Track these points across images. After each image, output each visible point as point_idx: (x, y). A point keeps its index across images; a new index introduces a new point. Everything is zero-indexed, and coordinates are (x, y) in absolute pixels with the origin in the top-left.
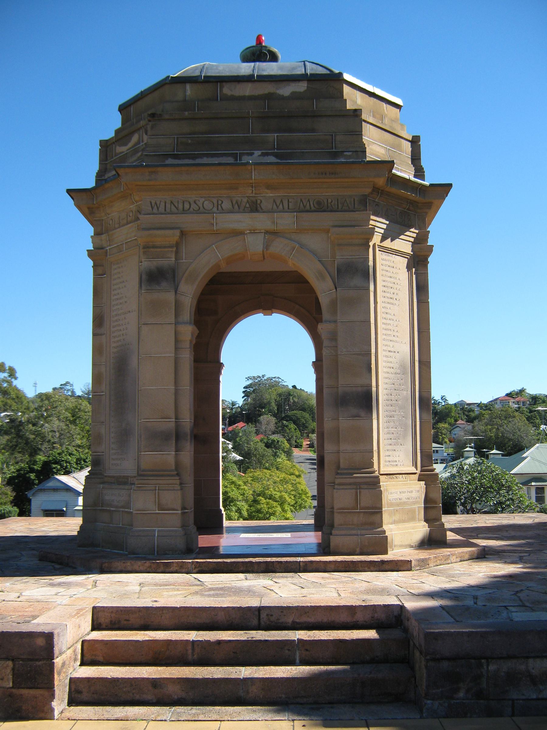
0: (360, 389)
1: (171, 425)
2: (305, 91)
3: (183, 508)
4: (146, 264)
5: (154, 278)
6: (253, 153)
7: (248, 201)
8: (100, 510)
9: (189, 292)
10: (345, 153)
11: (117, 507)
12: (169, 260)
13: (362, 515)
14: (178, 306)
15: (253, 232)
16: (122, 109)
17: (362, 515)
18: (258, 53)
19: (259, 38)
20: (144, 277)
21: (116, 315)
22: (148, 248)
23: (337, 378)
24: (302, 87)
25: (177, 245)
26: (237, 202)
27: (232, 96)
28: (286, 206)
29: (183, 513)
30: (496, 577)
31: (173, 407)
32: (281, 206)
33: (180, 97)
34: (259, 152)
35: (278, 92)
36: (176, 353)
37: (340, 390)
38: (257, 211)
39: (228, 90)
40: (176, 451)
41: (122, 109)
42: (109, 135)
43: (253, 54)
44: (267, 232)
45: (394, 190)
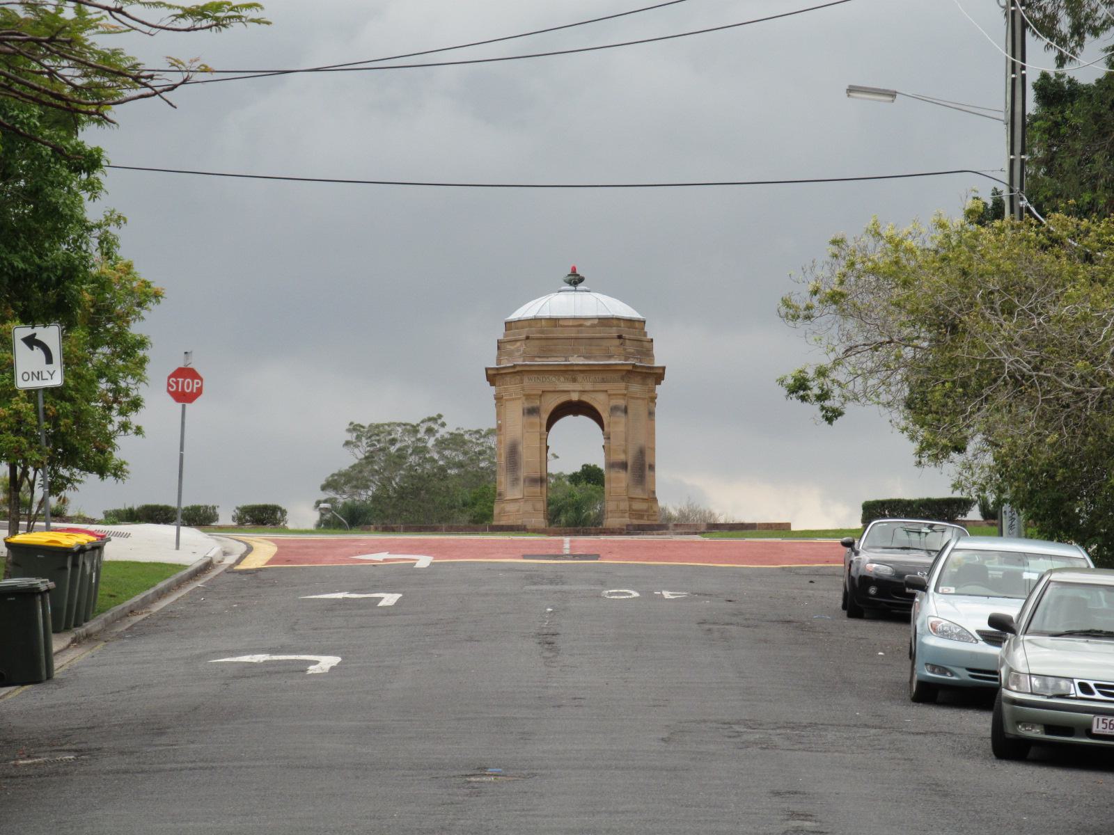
4: (527, 405)
12: (536, 403)
15: (574, 391)
19: (574, 269)
22: (528, 397)
24: (596, 322)
25: (541, 396)
39: (561, 323)
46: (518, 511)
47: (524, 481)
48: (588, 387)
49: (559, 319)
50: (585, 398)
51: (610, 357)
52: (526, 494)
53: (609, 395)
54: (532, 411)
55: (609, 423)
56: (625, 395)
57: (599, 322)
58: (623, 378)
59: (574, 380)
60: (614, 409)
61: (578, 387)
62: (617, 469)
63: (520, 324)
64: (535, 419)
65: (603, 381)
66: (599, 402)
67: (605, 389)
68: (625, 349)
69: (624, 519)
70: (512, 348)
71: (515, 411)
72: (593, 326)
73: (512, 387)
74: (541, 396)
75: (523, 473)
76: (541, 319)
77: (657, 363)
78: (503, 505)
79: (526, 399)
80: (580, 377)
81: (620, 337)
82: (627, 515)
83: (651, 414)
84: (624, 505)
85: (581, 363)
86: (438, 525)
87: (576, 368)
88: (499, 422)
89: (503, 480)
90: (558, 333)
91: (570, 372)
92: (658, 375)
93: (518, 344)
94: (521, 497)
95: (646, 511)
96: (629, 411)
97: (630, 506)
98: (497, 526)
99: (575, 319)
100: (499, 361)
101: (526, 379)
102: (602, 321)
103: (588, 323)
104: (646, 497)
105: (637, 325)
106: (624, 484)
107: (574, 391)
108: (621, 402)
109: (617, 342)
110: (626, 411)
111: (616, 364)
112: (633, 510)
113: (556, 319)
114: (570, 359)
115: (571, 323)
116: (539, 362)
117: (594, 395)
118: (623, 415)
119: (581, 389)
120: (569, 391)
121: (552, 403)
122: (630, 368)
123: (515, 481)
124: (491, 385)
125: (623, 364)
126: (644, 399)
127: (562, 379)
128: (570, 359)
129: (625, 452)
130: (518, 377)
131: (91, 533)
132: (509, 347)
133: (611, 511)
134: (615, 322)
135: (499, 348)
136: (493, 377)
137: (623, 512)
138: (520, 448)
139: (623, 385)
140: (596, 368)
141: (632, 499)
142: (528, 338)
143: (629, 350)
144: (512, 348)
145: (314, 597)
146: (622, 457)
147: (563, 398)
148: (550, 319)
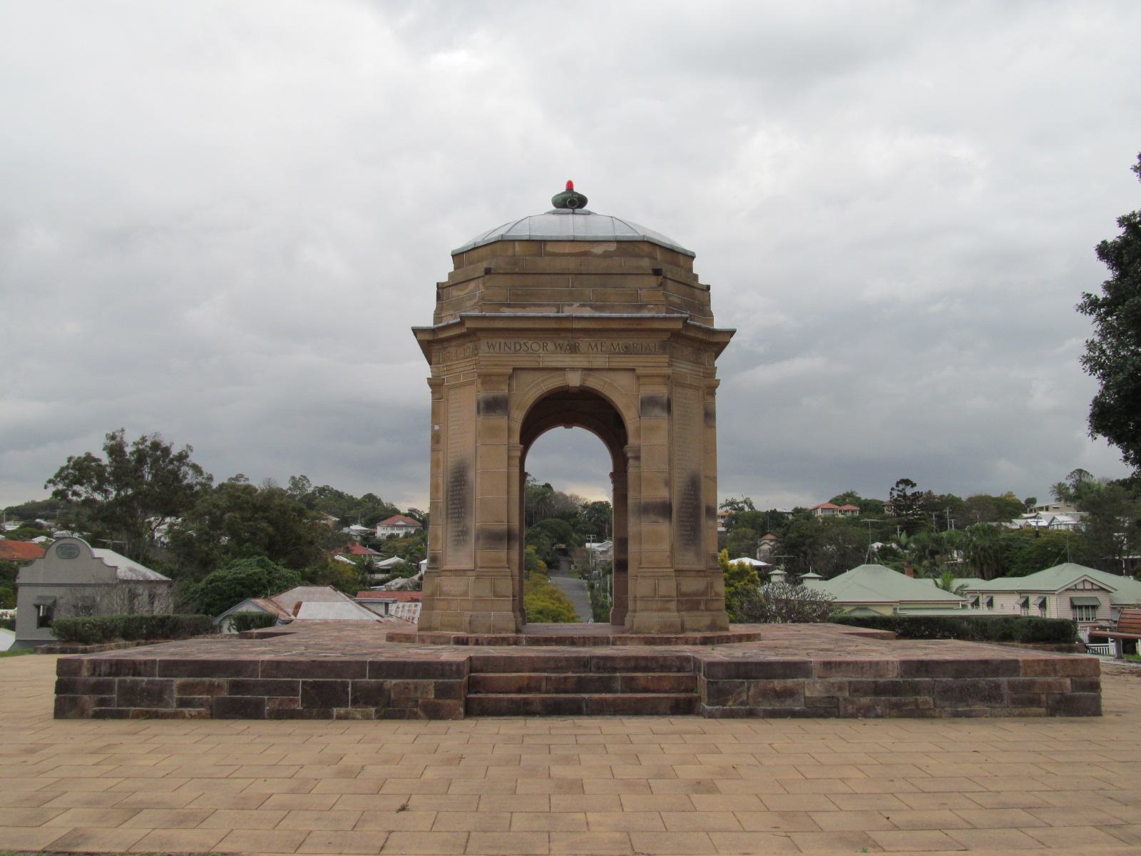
0: (658, 500)
1: (505, 527)
2: (615, 251)
3: (514, 596)
4: (484, 394)
5: (492, 406)
6: (572, 305)
7: (568, 345)
8: (438, 599)
9: (518, 416)
10: (649, 306)
11: (454, 596)
12: (502, 391)
13: (659, 602)
14: (509, 429)
15: (573, 369)
16: (457, 256)
17: (659, 602)
18: (571, 201)
19: (570, 185)
20: (482, 405)
21: (453, 434)
22: (486, 378)
23: (640, 492)
24: (613, 247)
25: (511, 377)
26: (559, 344)
27: (554, 253)
28: (599, 350)
29: (513, 600)
30: (558, 195)
31: (505, 511)
32: (595, 349)
33: (510, 253)
34: (578, 304)
35: (592, 250)
36: (508, 469)
37: (642, 502)
38: (576, 352)
39: (550, 248)
40: (508, 549)
41: (457, 256)
42: (444, 279)
43: (565, 200)
44: (585, 369)
45: (691, 334)
46: (465, 594)
47: (477, 538)
48: (600, 362)
49: (545, 241)
50: (594, 383)
51: (640, 307)
52: (479, 565)
53: (638, 377)
54: (492, 406)
55: (638, 430)
56: (668, 377)
57: (618, 248)
58: (664, 347)
59: (574, 349)
60: (648, 404)
61: (580, 361)
62: (654, 518)
63: (474, 254)
64: (500, 421)
65: (628, 351)
66: (622, 392)
67: (631, 365)
68: (666, 297)
69: (667, 614)
70: (461, 294)
71: (466, 401)
72: (607, 255)
73: (462, 364)
74: (511, 377)
75: (475, 523)
76: (514, 241)
77: (718, 324)
78: (438, 580)
79: (483, 383)
80: (584, 343)
81: (657, 272)
82: (673, 605)
83: (709, 416)
84: (667, 587)
85: (587, 315)
86: (936, 692)
87: (576, 325)
88: (437, 427)
89: (440, 533)
90: (544, 263)
91: (563, 333)
92: (716, 342)
93: (472, 285)
94: (471, 566)
95: (704, 593)
96: (674, 407)
97: (678, 585)
98: (520, 529)
99: (574, 241)
100: (438, 316)
101: (483, 346)
102: (624, 246)
103: (598, 250)
104: (702, 567)
105: (682, 260)
106: (666, 547)
107: (573, 369)
108: (661, 391)
109: (653, 281)
110: (668, 407)
111: (652, 319)
112: (684, 595)
113: (540, 241)
114: (566, 309)
115: (567, 249)
116: (508, 312)
117: (608, 377)
118: (665, 415)
119: (586, 365)
120: (563, 369)
121: (529, 392)
122: (679, 325)
123: (462, 534)
124: (432, 342)
125: (664, 319)
126: (697, 388)
127: (551, 346)
128: (566, 309)
129: (668, 483)
130: (471, 345)
131: (825, 613)
132: (456, 293)
133: (643, 598)
134: (646, 249)
135: (439, 297)
136: (431, 342)
137: (667, 599)
138: (471, 475)
139: (665, 359)
140: (615, 325)
141: (679, 572)
142: (488, 271)
143: (672, 299)
144: (461, 294)
145: (290, 679)
146: (662, 494)
147: (551, 383)
148: (530, 241)
